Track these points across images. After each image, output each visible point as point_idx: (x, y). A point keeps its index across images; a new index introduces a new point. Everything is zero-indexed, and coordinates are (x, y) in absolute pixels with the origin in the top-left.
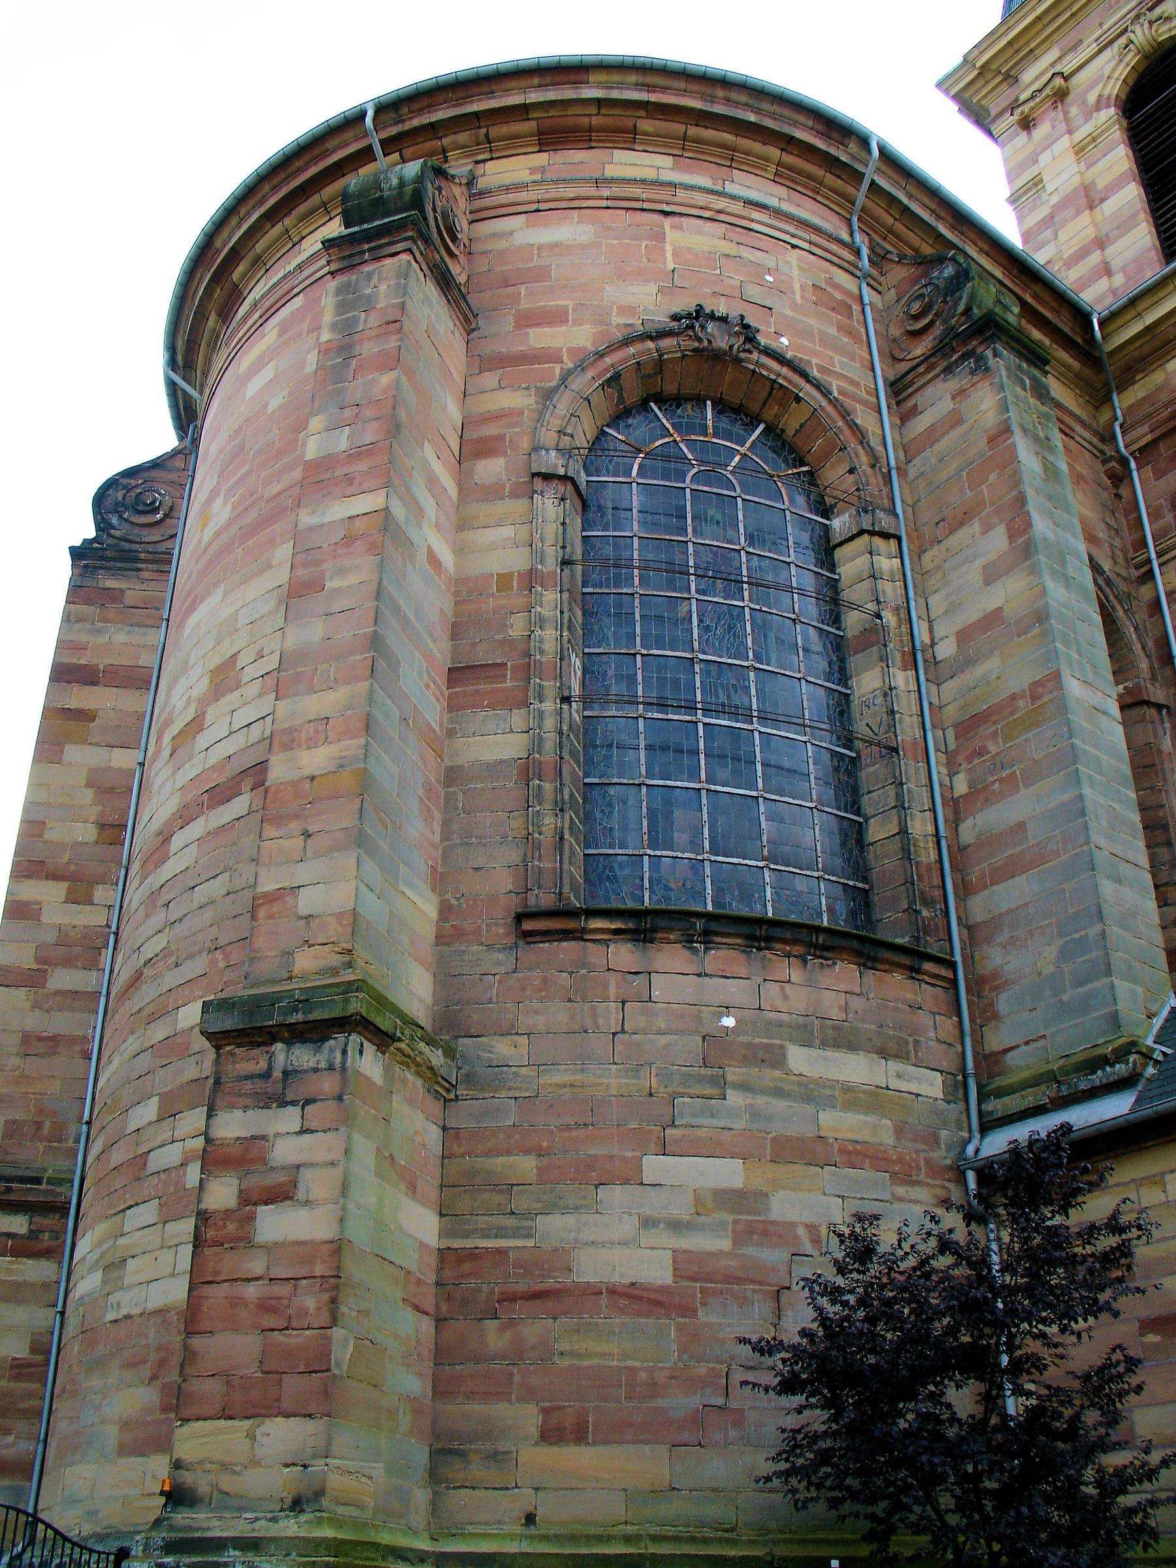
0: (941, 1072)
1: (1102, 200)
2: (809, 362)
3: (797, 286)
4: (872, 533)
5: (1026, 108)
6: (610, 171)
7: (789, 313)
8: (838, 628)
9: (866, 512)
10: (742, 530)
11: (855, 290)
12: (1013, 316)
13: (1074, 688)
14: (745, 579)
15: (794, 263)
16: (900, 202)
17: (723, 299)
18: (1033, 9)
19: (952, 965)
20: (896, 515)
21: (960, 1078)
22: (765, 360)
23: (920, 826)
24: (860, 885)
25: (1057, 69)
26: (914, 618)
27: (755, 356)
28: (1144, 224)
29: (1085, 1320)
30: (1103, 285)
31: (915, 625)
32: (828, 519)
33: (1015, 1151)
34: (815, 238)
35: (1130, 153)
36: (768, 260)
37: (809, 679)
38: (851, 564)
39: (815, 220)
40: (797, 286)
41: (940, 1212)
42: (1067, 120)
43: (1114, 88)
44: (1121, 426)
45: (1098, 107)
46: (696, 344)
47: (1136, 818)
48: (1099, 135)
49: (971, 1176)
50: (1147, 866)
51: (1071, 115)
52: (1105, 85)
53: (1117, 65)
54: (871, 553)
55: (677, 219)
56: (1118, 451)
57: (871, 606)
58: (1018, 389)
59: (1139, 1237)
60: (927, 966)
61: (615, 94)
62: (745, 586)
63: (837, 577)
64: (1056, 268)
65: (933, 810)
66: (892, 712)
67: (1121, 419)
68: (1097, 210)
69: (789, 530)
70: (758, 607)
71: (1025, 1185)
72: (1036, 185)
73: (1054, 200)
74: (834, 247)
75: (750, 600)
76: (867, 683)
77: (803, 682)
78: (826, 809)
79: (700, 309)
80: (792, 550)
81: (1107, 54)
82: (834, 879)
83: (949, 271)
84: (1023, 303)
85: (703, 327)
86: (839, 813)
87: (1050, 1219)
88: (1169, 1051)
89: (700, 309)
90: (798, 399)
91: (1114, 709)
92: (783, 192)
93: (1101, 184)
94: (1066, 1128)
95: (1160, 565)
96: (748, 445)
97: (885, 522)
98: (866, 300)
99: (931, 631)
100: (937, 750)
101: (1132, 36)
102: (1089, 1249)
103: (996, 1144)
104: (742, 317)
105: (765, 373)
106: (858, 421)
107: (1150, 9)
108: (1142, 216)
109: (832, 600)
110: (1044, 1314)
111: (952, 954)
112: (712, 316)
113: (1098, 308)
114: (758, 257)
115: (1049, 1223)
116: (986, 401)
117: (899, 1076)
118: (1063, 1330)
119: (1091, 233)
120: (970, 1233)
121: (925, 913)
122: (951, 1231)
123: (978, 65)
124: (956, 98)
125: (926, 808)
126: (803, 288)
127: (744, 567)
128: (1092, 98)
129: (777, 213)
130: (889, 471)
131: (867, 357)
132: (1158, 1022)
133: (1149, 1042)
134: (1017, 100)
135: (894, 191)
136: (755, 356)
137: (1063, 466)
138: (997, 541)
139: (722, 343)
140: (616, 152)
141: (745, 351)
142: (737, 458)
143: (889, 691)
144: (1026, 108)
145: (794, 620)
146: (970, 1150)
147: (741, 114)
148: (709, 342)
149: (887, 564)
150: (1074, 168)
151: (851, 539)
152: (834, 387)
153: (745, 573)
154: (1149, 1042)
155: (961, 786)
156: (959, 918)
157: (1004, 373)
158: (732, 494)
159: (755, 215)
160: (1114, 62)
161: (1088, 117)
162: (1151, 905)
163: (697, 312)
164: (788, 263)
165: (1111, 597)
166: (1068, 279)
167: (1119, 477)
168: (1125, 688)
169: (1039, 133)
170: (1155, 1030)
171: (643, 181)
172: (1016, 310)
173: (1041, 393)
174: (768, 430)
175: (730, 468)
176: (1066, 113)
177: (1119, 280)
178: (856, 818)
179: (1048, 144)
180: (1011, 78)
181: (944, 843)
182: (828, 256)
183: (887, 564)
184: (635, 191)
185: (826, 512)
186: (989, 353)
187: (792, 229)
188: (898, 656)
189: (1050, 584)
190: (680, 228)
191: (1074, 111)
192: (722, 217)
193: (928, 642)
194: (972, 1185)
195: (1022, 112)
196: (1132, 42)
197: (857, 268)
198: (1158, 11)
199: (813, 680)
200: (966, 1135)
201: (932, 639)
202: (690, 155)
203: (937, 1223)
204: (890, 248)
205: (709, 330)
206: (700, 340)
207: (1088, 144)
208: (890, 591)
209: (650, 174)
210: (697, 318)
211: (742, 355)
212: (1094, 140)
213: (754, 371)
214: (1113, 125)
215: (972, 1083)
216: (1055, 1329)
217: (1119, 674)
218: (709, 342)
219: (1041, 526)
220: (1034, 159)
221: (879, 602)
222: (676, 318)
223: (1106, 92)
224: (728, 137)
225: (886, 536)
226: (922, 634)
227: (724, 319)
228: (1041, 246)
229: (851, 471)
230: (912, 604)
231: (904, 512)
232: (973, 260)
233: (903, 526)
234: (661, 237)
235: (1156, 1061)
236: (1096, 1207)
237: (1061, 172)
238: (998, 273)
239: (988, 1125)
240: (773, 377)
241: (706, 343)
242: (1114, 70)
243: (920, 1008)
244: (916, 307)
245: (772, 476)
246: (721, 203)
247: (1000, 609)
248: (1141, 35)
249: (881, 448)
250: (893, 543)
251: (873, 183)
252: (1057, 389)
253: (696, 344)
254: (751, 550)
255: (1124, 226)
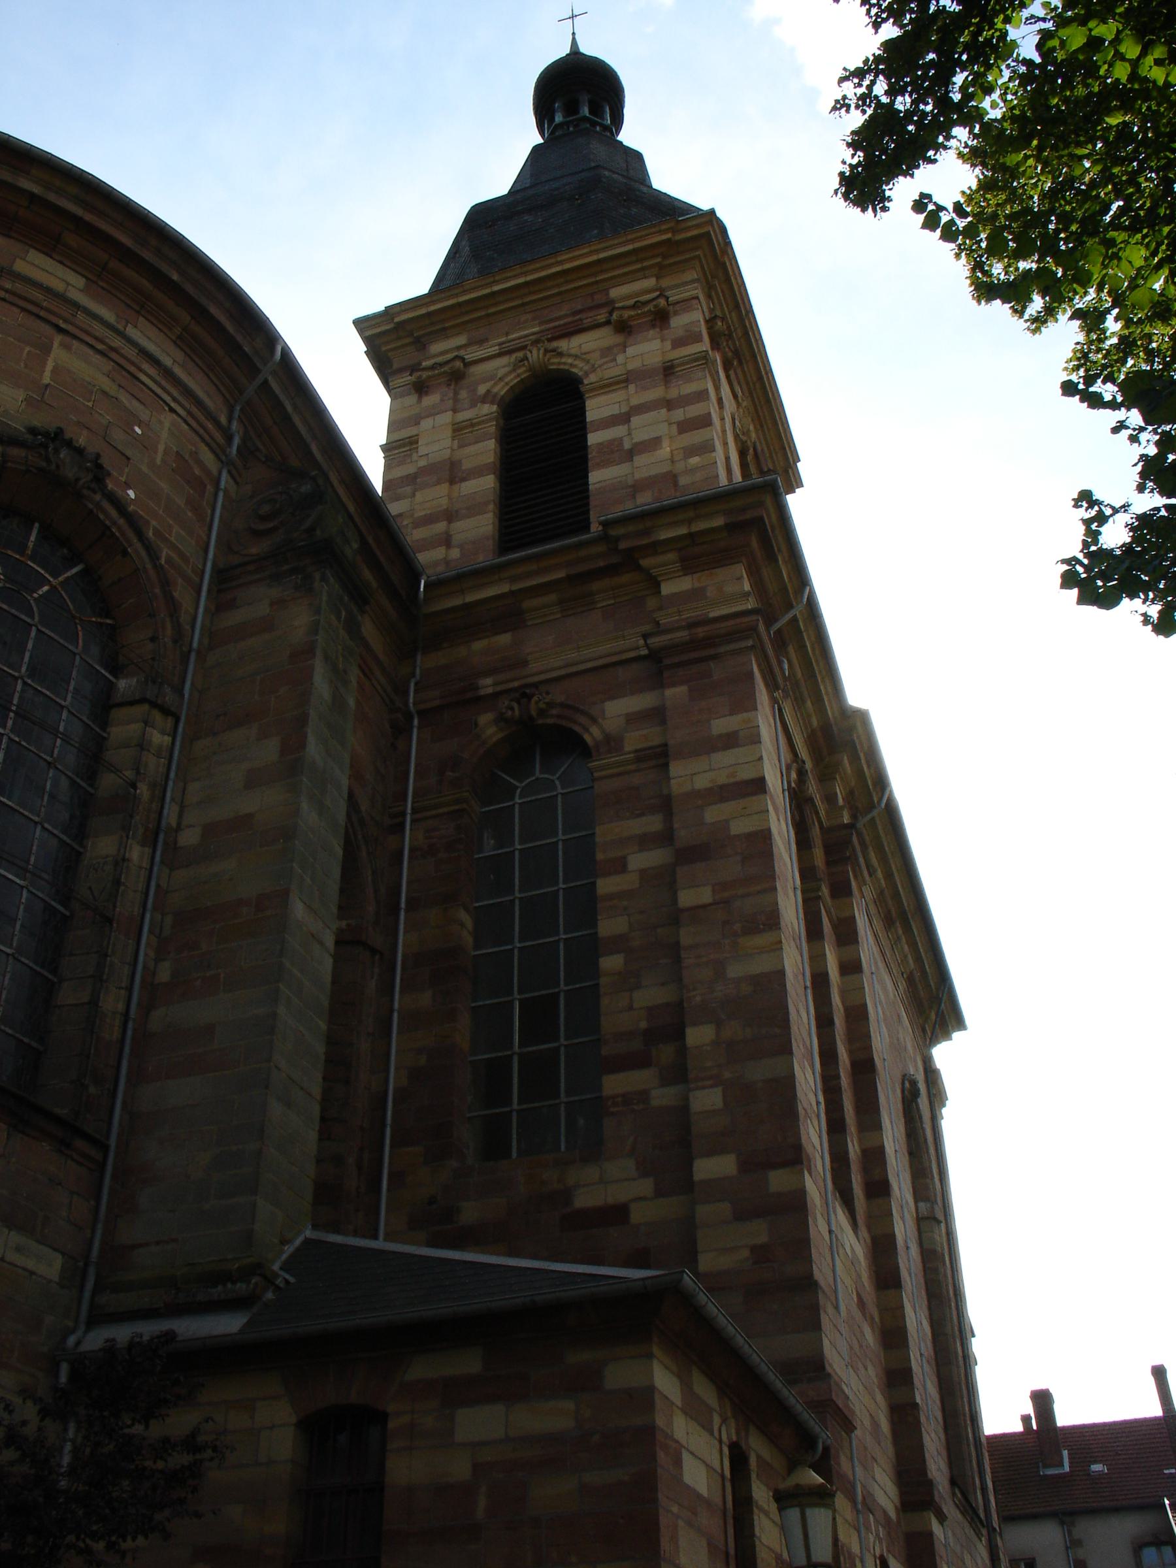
0: (63, 1254)
1: (464, 480)
2: (148, 522)
3: (161, 448)
4: (154, 705)
5: (425, 375)
6: (20, 266)
7: (144, 469)
8: (91, 786)
9: (154, 682)
10: (26, 659)
11: (215, 472)
12: (351, 549)
13: (298, 910)
14: (14, 708)
15: (167, 425)
16: (284, 408)
17: (85, 432)
18: (457, 295)
19: (105, 1148)
20: (182, 696)
21: (81, 1264)
22: (106, 505)
23: (112, 1002)
24: (34, 1044)
25: (462, 353)
26: (168, 799)
27: (98, 497)
28: (490, 515)
29: (134, 1539)
30: (439, 553)
31: (167, 806)
32: (116, 677)
33: (110, 1348)
34: (195, 410)
35: (498, 450)
36: (144, 414)
37: (46, 825)
38: (124, 728)
39: (201, 394)
40: (161, 448)
41: (17, 1401)
42: (456, 400)
43: (501, 390)
44: (416, 684)
45: (484, 399)
46: (44, 464)
47: (320, 1049)
48: (479, 423)
49: (64, 1369)
50: (319, 1098)
51: (460, 397)
52: (495, 384)
53: (510, 372)
54: (146, 723)
55: (68, 339)
56: (406, 704)
57: (129, 774)
58: (333, 617)
59: (212, 1459)
60: (79, 1143)
61: (52, 197)
62: (12, 715)
63: (105, 735)
64: (405, 523)
65: (130, 989)
66: (117, 882)
67: (418, 677)
68: (456, 487)
69: (74, 673)
70: (17, 739)
71: (109, 1389)
72: (411, 443)
73: (422, 463)
74: (210, 426)
75: (11, 730)
76: (103, 847)
77: (39, 828)
78: (23, 959)
79: (60, 432)
80: (70, 695)
81: (504, 360)
82: (10, 1031)
83: (306, 488)
84: (364, 542)
85: (57, 451)
86: (35, 967)
87: (129, 1427)
88: (292, 1279)
89: (60, 432)
90: (125, 553)
91: (329, 940)
92: (179, 356)
93: (467, 465)
94: (170, 1336)
95: (413, 821)
96: (61, 579)
97: (169, 698)
98: (223, 485)
99: (180, 816)
100: (151, 932)
101: (529, 355)
102: (160, 1465)
103: (95, 1340)
104: (98, 456)
105: (102, 516)
106: (176, 594)
107: (550, 340)
108: (491, 507)
109: (94, 756)
110: (95, 1528)
111: (108, 1137)
112: (69, 444)
113: (429, 572)
114: (135, 406)
115: (127, 1431)
116: (299, 617)
117: (18, 1249)
118: (111, 1546)
119: (444, 502)
120: (40, 1429)
121: (92, 1090)
122: (24, 1423)
123: (397, 320)
124: (367, 340)
125: (123, 985)
126: (166, 452)
127: (17, 696)
128: (482, 389)
129: (168, 373)
130: (190, 652)
131: (205, 538)
132: (289, 1250)
133: (276, 1267)
134: (420, 364)
135: (282, 397)
136: (98, 497)
137: (352, 702)
138: (269, 752)
139: (70, 473)
140: (32, 251)
141: (89, 488)
142: (46, 588)
143: (121, 861)
144: (425, 375)
145: (49, 763)
146: (72, 1340)
147: (165, 268)
148: (58, 467)
149: (158, 738)
150: (447, 442)
151: (132, 703)
152: (164, 554)
153: (15, 701)
154: (276, 1267)
155: (164, 974)
156: (124, 1103)
157: (325, 598)
158: (29, 620)
159: (146, 366)
160: (507, 369)
161: (473, 405)
162: (312, 1136)
163: (56, 434)
164: (160, 422)
165: (360, 837)
166: (413, 536)
167: (401, 730)
168: (348, 925)
169: (431, 400)
170: (284, 1257)
171: (48, 291)
172: (355, 546)
173: (352, 628)
174: (86, 572)
175: (35, 595)
176: (456, 393)
177: (455, 553)
178: (50, 977)
179: (432, 413)
180: (421, 344)
181: (130, 1025)
182: (201, 431)
183: (158, 738)
184: (38, 296)
185: (116, 670)
186: (317, 576)
187: (175, 394)
188: (141, 831)
189: (305, 806)
190: (68, 348)
191: (463, 394)
192: (113, 355)
193: (174, 825)
194: (63, 1379)
195: (420, 377)
196: (527, 359)
197: (224, 452)
198: (555, 344)
199: (50, 828)
200: (71, 1324)
201: (179, 824)
202: (105, 285)
203: (11, 1412)
204: (261, 447)
205: (62, 456)
206: (48, 460)
207: (466, 427)
208: (153, 765)
209: (59, 286)
210: (53, 440)
211: (85, 492)
212: (472, 425)
213: (91, 511)
214: (490, 420)
215: (92, 1271)
216: (100, 1546)
217: (343, 910)
218: (58, 467)
219: (313, 749)
220: (416, 420)
221: (138, 773)
222: (33, 431)
223: (495, 390)
224: (146, 284)
225: (166, 711)
226: (170, 814)
227: (80, 451)
228: (398, 498)
229: (153, 639)
230: (171, 783)
231: (191, 695)
232: (332, 486)
233: (185, 707)
234: (46, 350)
235: (278, 1288)
236: (179, 1422)
237: (436, 442)
238: (352, 508)
239: (97, 1319)
240: (107, 522)
241: (53, 467)
242: (506, 375)
243: (60, 1184)
244: (266, 509)
245: (74, 617)
246: (117, 342)
247: (250, 816)
248: (535, 355)
249: (188, 627)
250: (170, 721)
251: (266, 382)
252: (368, 629)
253: (44, 464)
254: (29, 681)
255: (474, 509)
